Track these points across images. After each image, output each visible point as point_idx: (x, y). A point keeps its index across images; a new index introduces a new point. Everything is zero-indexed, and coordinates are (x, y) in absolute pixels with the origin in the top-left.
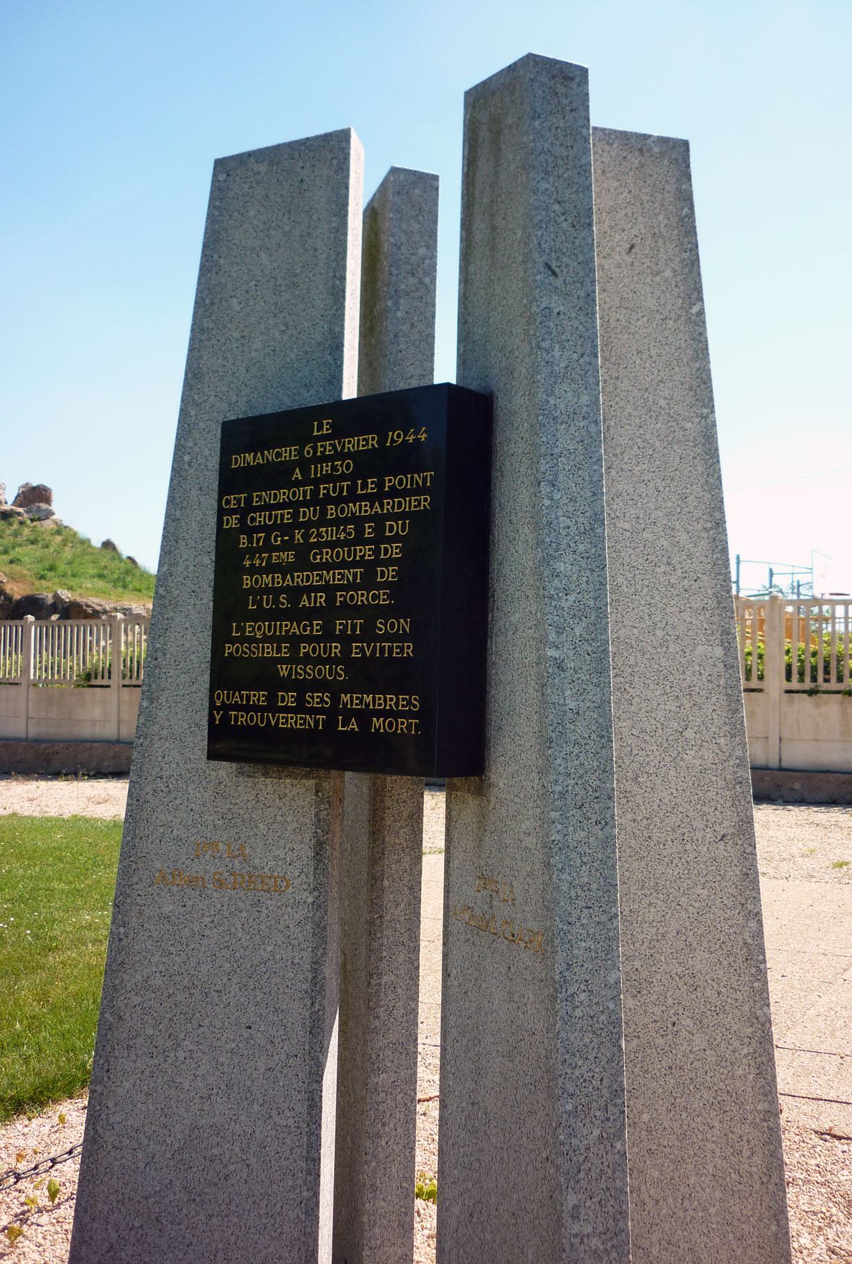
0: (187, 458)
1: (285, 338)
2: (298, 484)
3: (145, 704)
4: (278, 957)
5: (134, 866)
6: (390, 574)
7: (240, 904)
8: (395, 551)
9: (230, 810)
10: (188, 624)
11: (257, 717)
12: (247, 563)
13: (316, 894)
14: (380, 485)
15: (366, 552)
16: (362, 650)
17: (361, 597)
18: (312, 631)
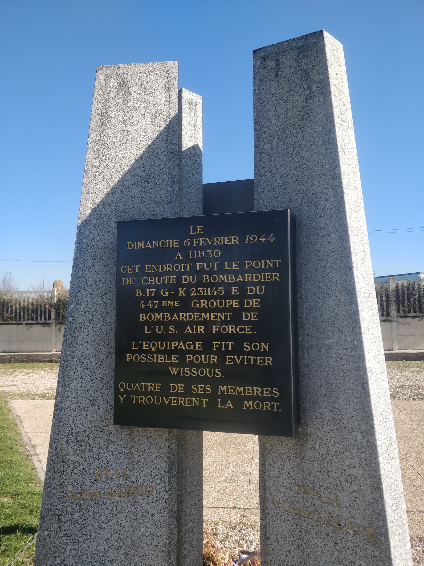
0: (85, 241)
1: (144, 175)
2: (179, 261)
3: (60, 389)
4: (148, 533)
5: (54, 491)
6: (252, 316)
7: (124, 505)
8: (255, 303)
9: (117, 449)
10: (88, 340)
11: (153, 399)
12: (143, 306)
13: (170, 492)
14: (242, 265)
15: (234, 303)
16: (234, 360)
17: (231, 329)
18: (195, 347)
